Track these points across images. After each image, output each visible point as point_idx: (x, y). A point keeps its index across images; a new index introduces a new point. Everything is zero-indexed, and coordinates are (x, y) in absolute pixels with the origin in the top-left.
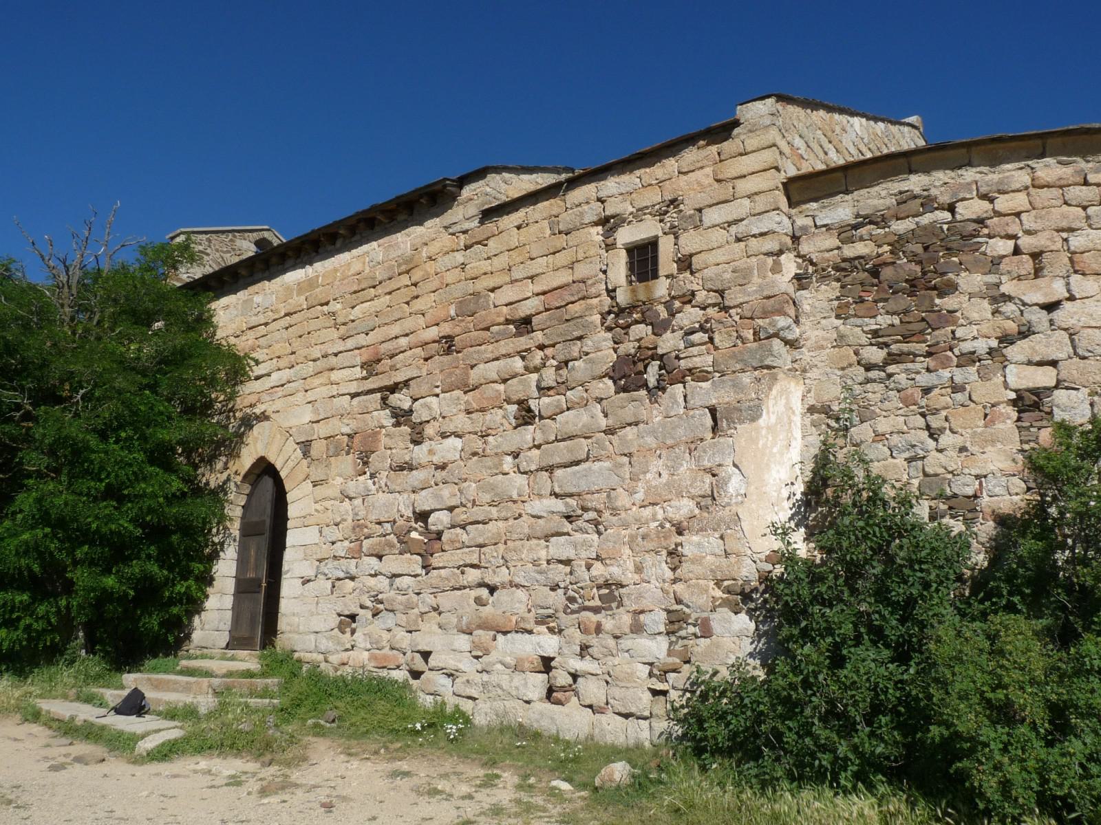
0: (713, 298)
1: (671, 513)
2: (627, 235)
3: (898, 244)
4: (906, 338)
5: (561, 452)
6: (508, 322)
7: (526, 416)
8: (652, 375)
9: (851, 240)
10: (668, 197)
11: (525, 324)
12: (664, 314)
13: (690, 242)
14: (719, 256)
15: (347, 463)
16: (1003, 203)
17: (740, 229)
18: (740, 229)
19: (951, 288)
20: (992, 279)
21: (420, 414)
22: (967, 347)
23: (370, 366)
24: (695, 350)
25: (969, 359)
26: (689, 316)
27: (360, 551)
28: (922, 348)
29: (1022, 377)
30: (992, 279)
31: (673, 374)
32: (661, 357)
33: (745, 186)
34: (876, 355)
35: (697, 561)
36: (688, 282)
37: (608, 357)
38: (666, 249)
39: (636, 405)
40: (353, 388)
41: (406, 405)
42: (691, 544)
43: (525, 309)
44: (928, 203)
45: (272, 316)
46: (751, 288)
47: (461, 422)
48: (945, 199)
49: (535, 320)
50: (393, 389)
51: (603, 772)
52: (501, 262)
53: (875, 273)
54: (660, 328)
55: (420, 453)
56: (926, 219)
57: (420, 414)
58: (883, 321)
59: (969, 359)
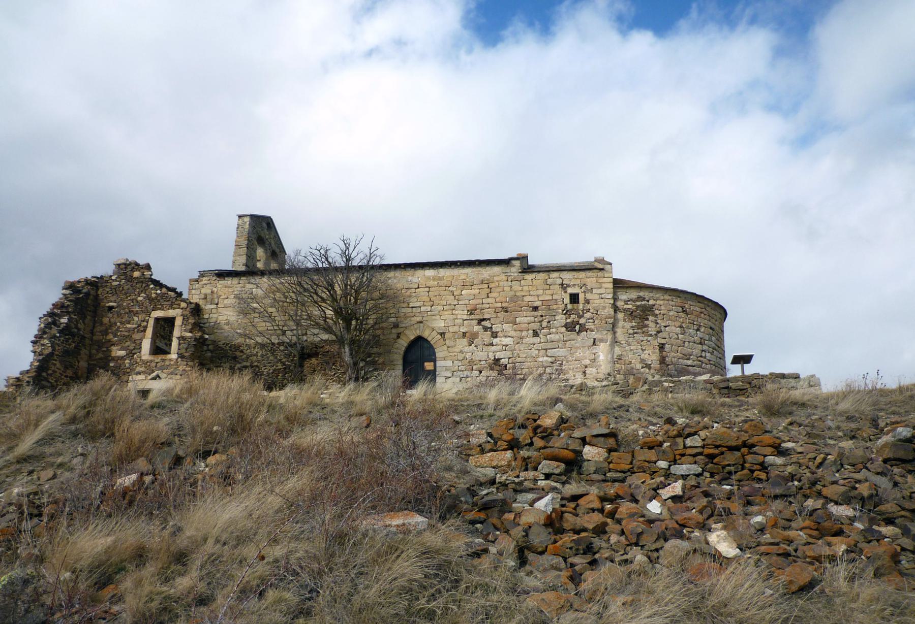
0: (596, 312)
1: (583, 363)
2: (570, 290)
3: (638, 307)
4: (638, 329)
5: (550, 345)
6: (530, 307)
7: (536, 334)
8: (577, 327)
9: (627, 304)
10: (583, 283)
11: (536, 309)
12: (581, 313)
13: (589, 296)
14: (596, 301)
15: (465, 341)
16: (658, 302)
17: (603, 296)
18: (603, 296)
19: (647, 319)
20: (656, 319)
21: (495, 328)
22: (650, 333)
23: (471, 312)
24: (590, 324)
25: (651, 335)
26: (588, 315)
27: (473, 369)
28: (641, 331)
29: (660, 341)
30: (656, 319)
31: (583, 329)
32: (580, 324)
33: (604, 285)
34: (631, 331)
35: (591, 374)
36: (588, 306)
37: (563, 322)
38: (581, 297)
39: (573, 335)
40: (465, 317)
41: (489, 326)
42: (588, 371)
43: (536, 304)
44: (644, 299)
45: (720, 366)
46: (606, 311)
47: (512, 333)
48: (647, 299)
49: (539, 308)
50: (484, 320)
51: (274, 501)
52: (526, 288)
53: (632, 313)
54: (581, 317)
55: (495, 341)
56: (643, 303)
57: (495, 328)
58: (634, 324)
59: (651, 335)
